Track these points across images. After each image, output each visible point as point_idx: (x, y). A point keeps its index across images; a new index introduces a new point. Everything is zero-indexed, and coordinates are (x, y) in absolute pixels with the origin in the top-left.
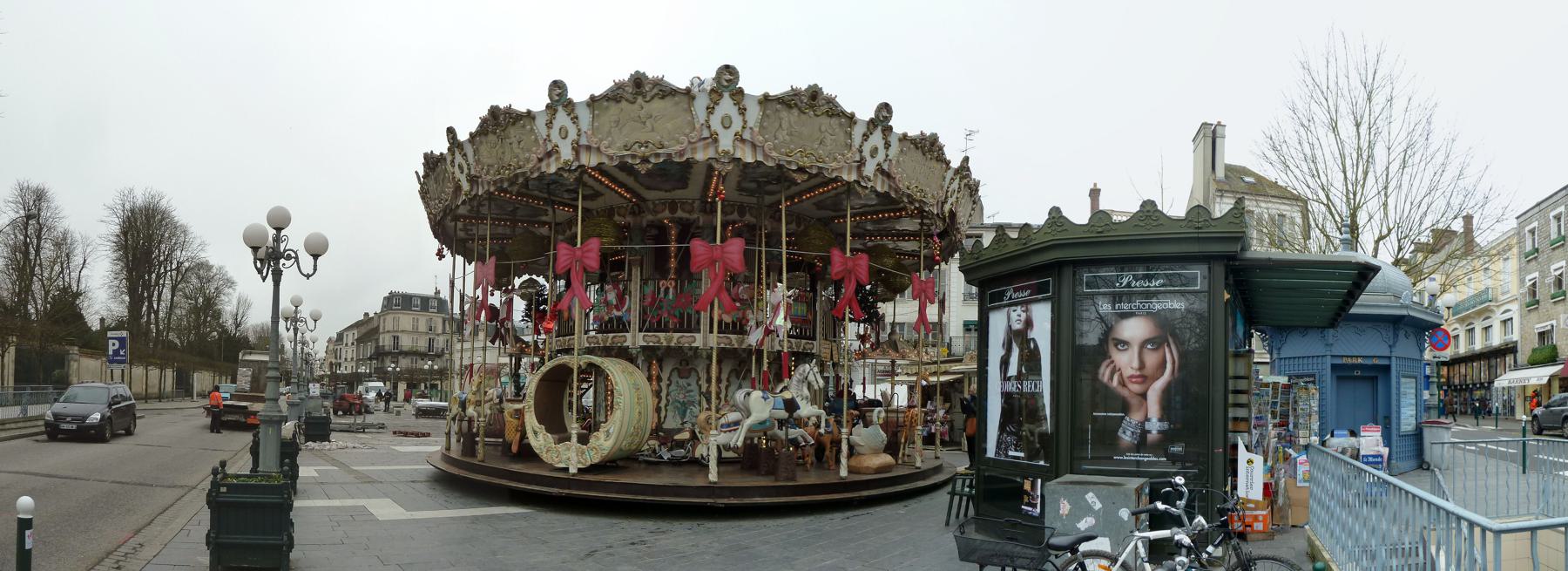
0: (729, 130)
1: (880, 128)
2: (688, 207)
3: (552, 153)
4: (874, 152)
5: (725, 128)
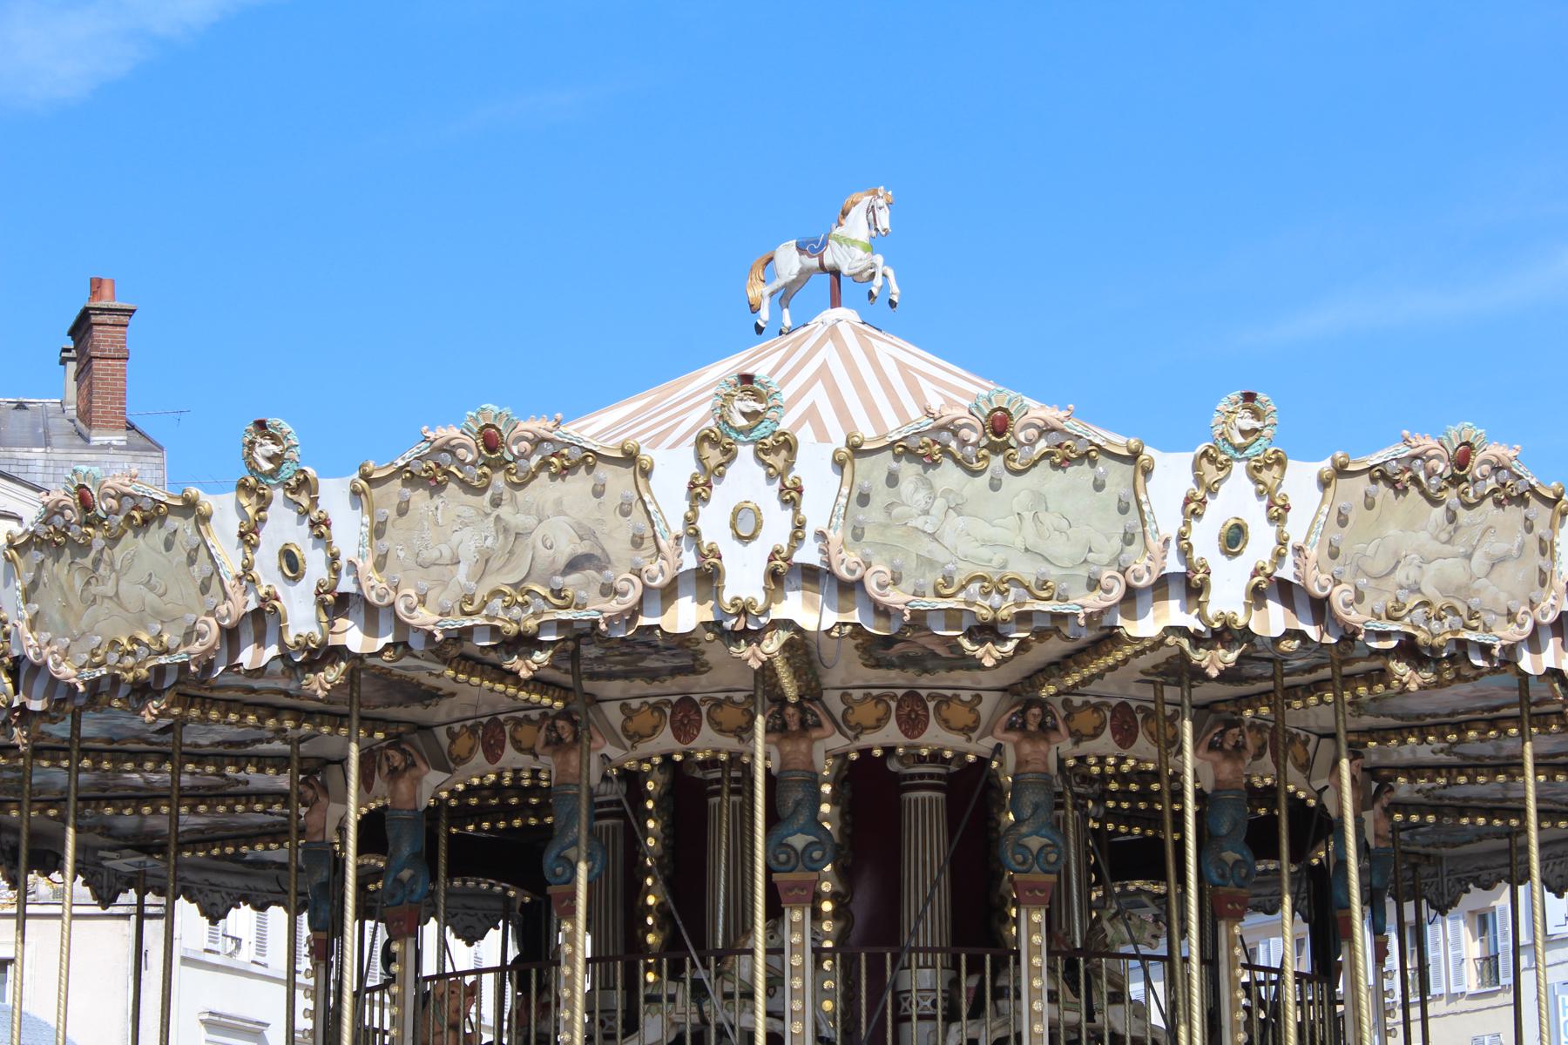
0: (753, 544)
1: (1239, 469)
2: (960, 715)
3: (263, 619)
4: (1234, 538)
5: (740, 538)
